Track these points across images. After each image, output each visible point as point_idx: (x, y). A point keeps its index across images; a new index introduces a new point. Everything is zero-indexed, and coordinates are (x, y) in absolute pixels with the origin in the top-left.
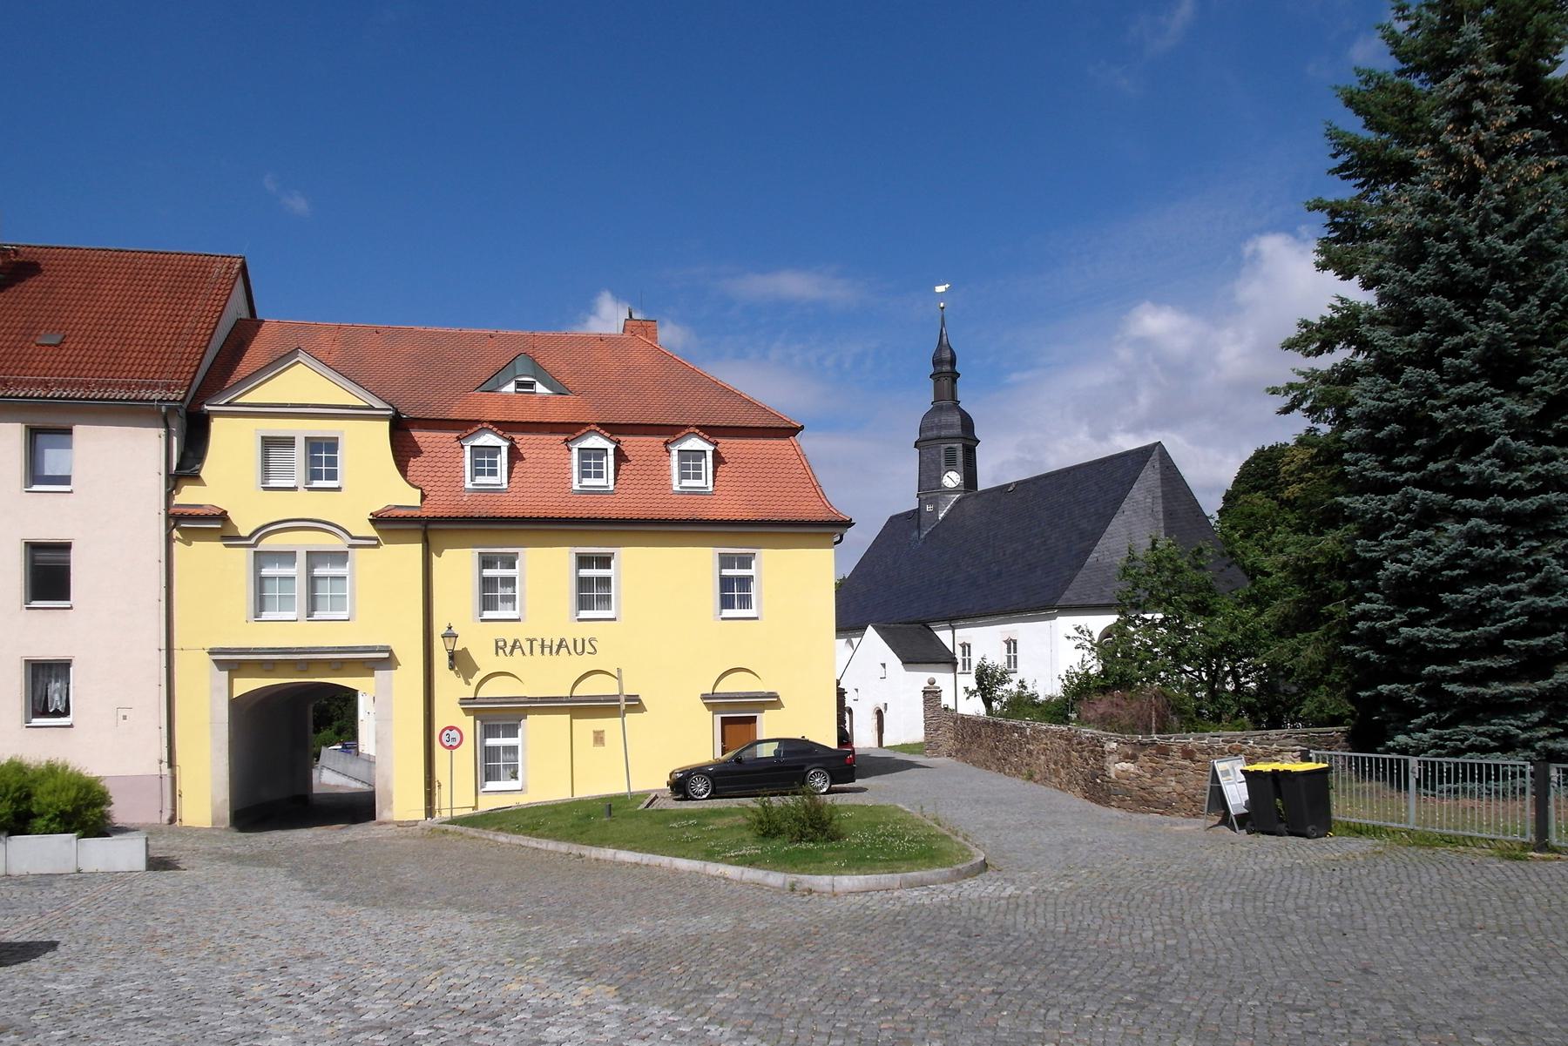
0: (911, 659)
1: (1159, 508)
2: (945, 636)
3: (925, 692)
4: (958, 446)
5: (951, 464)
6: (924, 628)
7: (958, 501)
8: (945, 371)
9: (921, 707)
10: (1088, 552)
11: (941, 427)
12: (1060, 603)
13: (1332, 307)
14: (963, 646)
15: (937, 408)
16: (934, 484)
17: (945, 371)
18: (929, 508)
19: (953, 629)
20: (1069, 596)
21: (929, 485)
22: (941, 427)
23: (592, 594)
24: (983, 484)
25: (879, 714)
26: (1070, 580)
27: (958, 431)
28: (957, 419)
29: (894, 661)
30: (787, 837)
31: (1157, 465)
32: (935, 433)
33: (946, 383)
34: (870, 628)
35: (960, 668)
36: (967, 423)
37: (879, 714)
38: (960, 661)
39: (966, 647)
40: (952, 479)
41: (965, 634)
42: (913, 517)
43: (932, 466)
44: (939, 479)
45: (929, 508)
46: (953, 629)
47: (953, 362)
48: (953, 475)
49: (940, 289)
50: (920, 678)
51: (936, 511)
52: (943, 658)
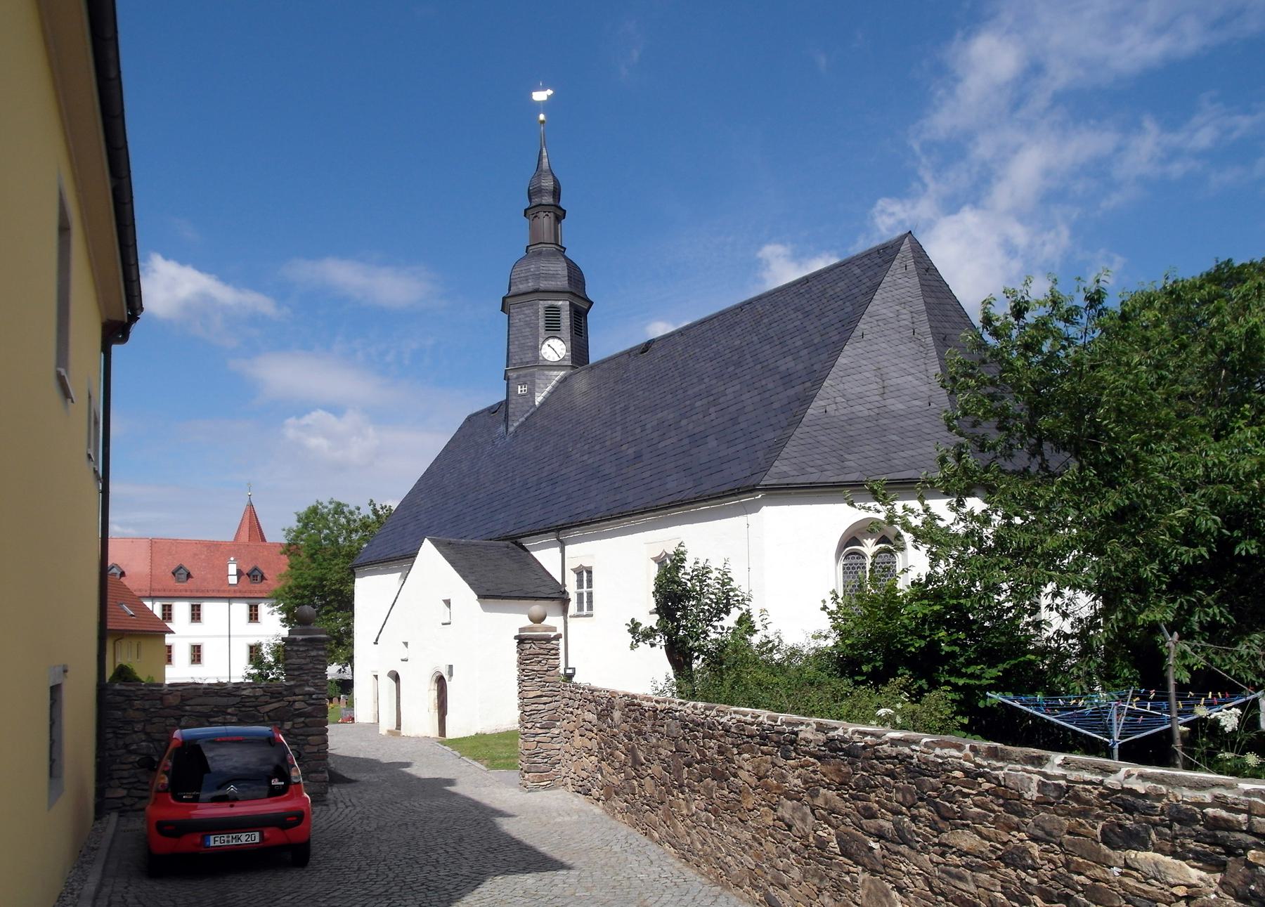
0: (491, 593)
1: (926, 328)
2: (547, 557)
3: (521, 640)
4: (563, 304)
5: (553, 327)
6: (516, 543)
7: (563, 381)
8: (547, 205)
9: (513, 672)
10: (807, 400)
11: (537, 277)
12: (767, 481)
13: (706, 571)
14: (578, 572)
15: (533, 252)
16: (529, 356)
17: (547, 205)
18: (521, 390)
19: (562, 545)
20: (781, 469)
21: (522, 364)
22: (537, 277)
23: (196, 616)
24: (597, 353)
25: (441, 681)
26: (781, 444)
27: (562, 283)
28: (561, 269)
29: (464, 594)
30: (940, 700)
31: (911, 266)
32: (531, 285)
33: (546, 221)
34: (428, 550)
35: (573, 608)
36: (576, 276)
37: (441, 681)
38: (573, 597)
39: (584, 574)
40: (555, 350)
41: (582, 552)
42: (500, 411)
43: (527, 331)
44: (536, 348)
45: (521, 390)
46: (562, 545)
47: (556, 193)
48: (556, 343)
49: (540, 96)
50: (514, 620)
51: (531, 393)
52: (546, 591)
